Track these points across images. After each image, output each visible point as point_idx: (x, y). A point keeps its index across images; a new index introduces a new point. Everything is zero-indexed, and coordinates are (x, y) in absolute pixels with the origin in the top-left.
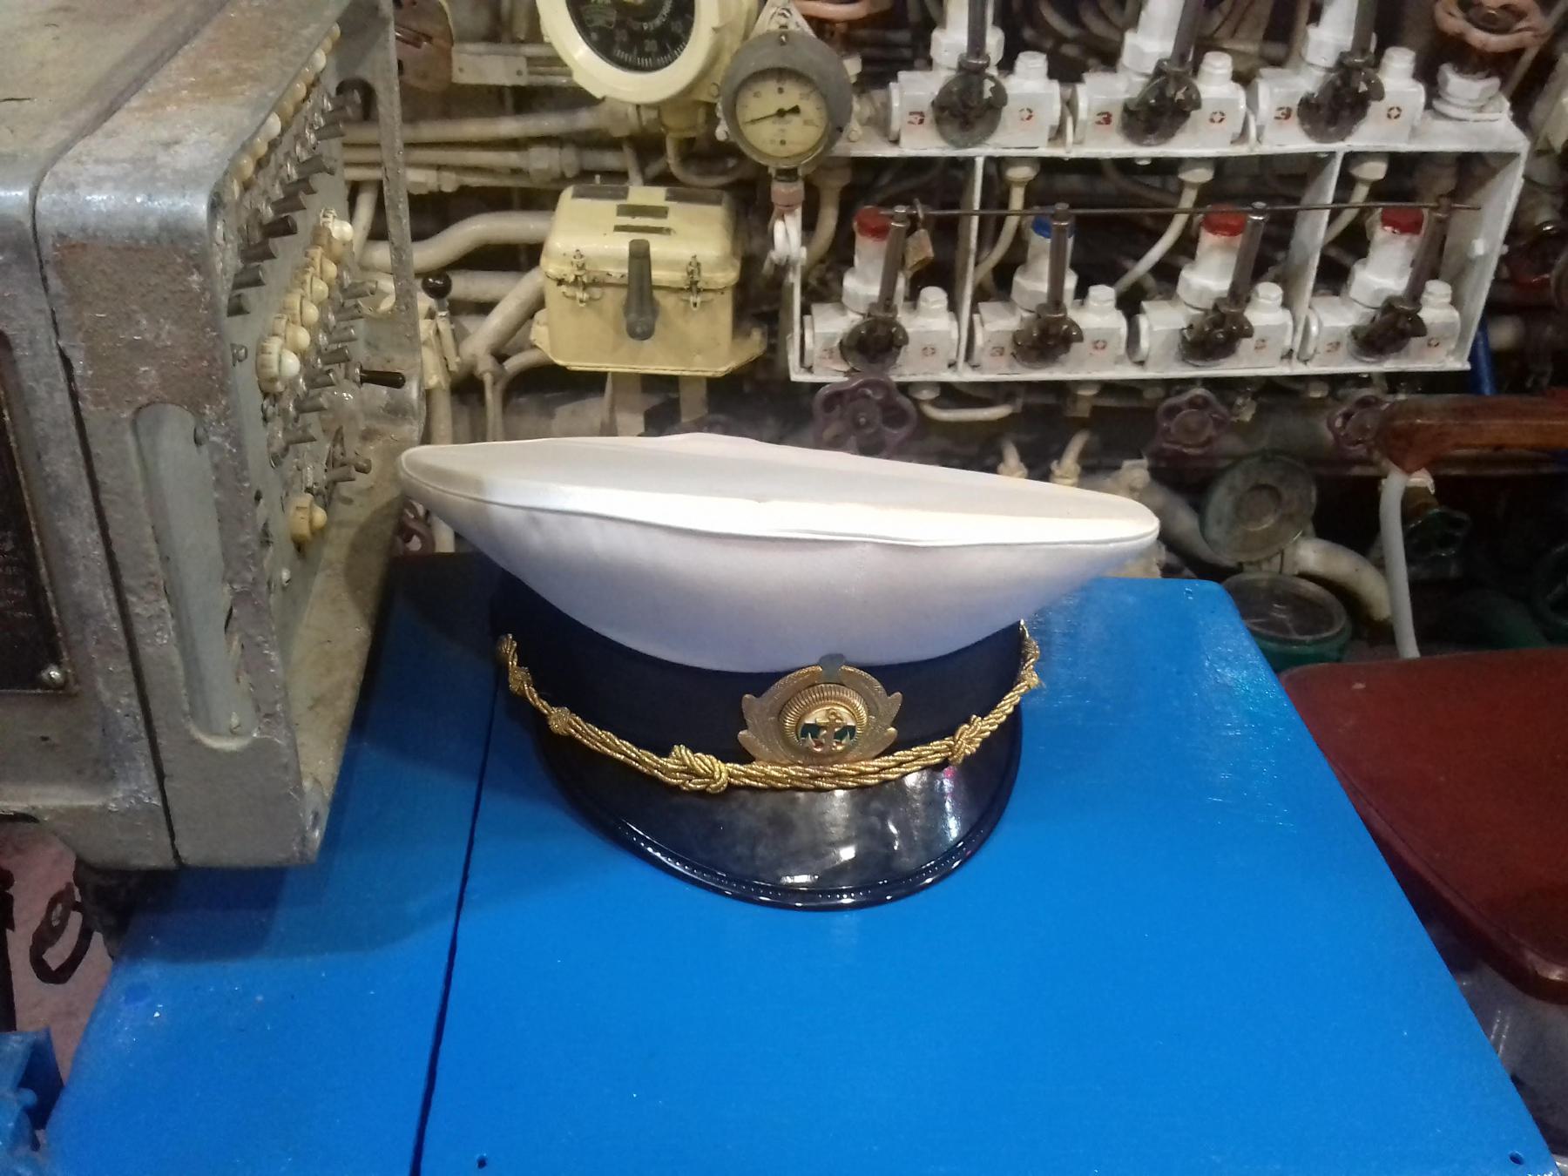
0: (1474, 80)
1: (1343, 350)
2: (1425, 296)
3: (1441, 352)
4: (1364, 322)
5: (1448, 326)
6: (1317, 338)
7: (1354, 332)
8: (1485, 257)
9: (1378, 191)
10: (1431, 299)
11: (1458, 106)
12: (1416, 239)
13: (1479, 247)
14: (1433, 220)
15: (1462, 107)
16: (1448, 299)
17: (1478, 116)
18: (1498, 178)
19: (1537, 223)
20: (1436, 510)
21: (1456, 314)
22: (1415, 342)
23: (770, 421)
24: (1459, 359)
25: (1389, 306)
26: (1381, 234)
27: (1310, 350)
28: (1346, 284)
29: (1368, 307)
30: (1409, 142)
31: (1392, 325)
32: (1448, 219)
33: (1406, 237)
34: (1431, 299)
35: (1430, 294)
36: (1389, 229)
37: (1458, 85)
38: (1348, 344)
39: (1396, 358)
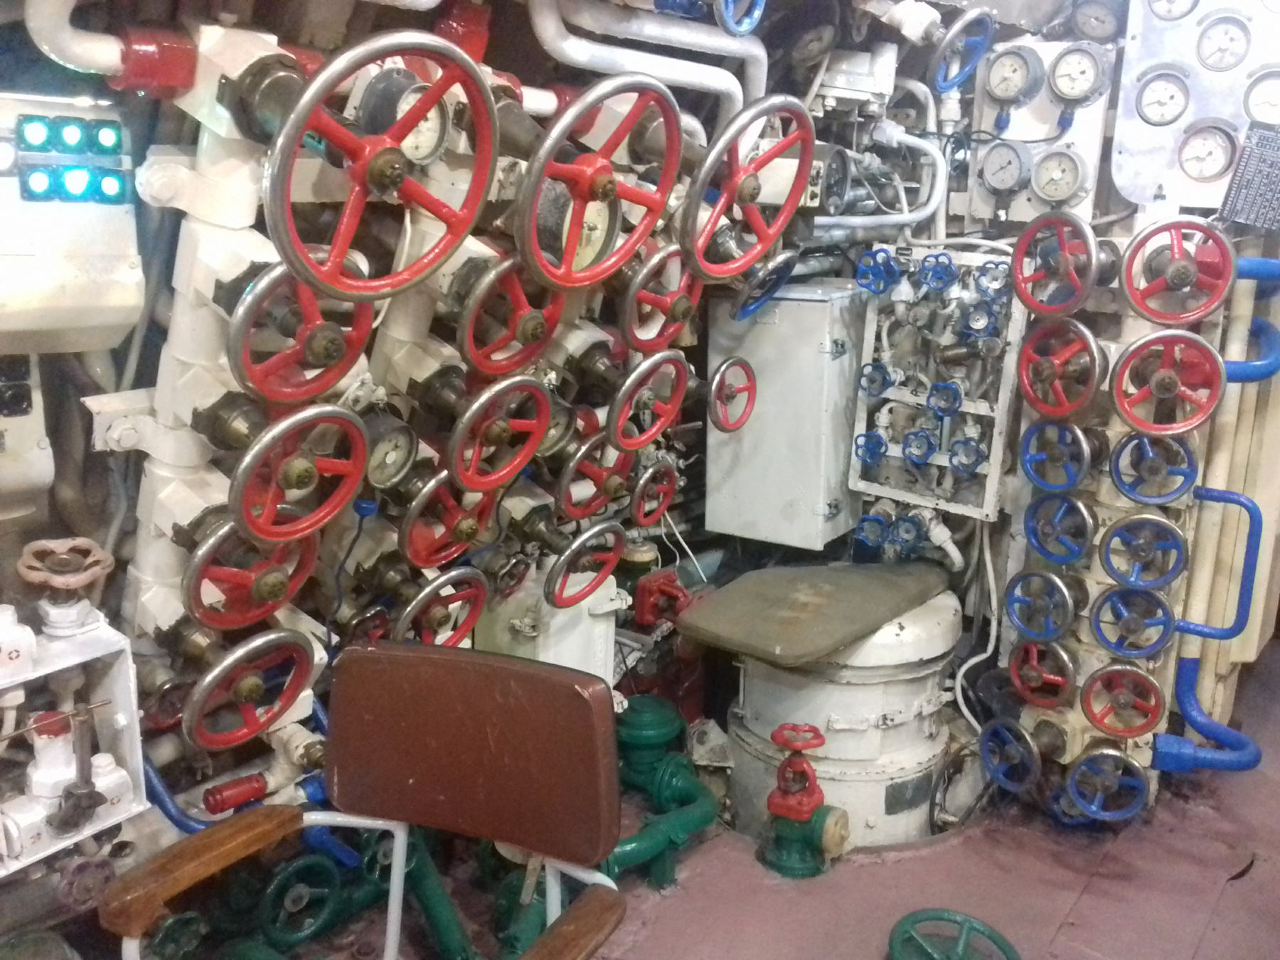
0: (70, 606)
1: (45, 836)
2: (94, 770)
3: (122, 806)
4: (54, 810)
5: (121, 785)
6: (19, 837)
7: (50, 821)
8: (128, 726)
9: (22, 710)
10: (100, 770)
11: (64, 628)
12: (70, 736)
13: (121, 720)
14: (531, 160)
15: (68, 628)
16: (114, 765)
17: (83, 630)
18: (115, 668)
19: (158, 683)
20: (170, 921)
21: (124, 772)
22: (100, 809)
23: (721, 250)
24: (140, 803)
25: (69, 794)
26: (40, 742)
27: (17, 848)
28: (125, 620)
29: (51, 798)
30: (34, 671)
31: (76, 807)
32: (524, 259)
33: (61, 738)
34: (100, 770)
35: (97, 767)
36: (45, 736)
37: (55, 613)
38: (45, 830)
39: (91, 823)
